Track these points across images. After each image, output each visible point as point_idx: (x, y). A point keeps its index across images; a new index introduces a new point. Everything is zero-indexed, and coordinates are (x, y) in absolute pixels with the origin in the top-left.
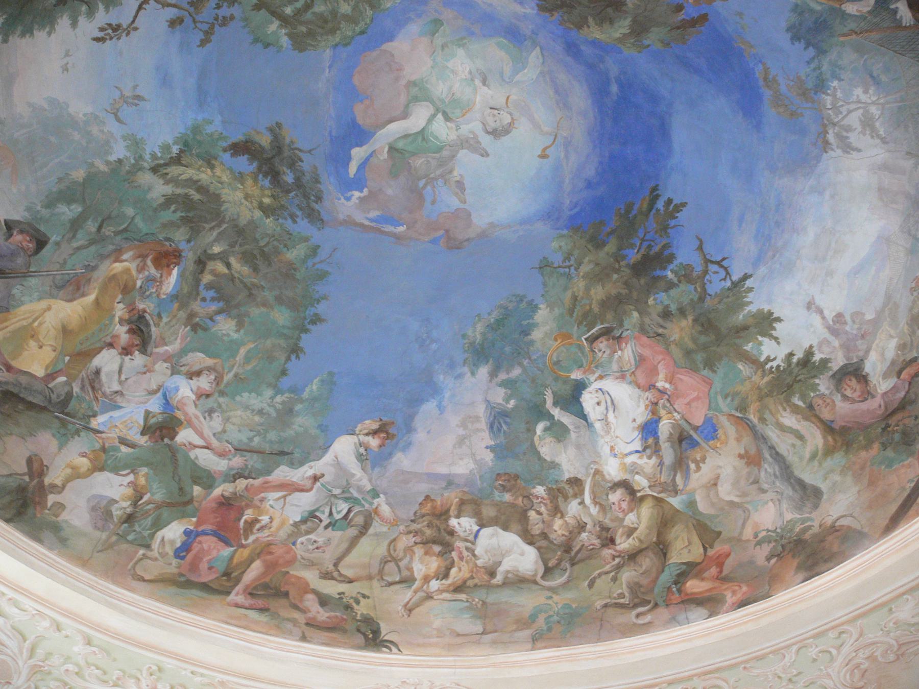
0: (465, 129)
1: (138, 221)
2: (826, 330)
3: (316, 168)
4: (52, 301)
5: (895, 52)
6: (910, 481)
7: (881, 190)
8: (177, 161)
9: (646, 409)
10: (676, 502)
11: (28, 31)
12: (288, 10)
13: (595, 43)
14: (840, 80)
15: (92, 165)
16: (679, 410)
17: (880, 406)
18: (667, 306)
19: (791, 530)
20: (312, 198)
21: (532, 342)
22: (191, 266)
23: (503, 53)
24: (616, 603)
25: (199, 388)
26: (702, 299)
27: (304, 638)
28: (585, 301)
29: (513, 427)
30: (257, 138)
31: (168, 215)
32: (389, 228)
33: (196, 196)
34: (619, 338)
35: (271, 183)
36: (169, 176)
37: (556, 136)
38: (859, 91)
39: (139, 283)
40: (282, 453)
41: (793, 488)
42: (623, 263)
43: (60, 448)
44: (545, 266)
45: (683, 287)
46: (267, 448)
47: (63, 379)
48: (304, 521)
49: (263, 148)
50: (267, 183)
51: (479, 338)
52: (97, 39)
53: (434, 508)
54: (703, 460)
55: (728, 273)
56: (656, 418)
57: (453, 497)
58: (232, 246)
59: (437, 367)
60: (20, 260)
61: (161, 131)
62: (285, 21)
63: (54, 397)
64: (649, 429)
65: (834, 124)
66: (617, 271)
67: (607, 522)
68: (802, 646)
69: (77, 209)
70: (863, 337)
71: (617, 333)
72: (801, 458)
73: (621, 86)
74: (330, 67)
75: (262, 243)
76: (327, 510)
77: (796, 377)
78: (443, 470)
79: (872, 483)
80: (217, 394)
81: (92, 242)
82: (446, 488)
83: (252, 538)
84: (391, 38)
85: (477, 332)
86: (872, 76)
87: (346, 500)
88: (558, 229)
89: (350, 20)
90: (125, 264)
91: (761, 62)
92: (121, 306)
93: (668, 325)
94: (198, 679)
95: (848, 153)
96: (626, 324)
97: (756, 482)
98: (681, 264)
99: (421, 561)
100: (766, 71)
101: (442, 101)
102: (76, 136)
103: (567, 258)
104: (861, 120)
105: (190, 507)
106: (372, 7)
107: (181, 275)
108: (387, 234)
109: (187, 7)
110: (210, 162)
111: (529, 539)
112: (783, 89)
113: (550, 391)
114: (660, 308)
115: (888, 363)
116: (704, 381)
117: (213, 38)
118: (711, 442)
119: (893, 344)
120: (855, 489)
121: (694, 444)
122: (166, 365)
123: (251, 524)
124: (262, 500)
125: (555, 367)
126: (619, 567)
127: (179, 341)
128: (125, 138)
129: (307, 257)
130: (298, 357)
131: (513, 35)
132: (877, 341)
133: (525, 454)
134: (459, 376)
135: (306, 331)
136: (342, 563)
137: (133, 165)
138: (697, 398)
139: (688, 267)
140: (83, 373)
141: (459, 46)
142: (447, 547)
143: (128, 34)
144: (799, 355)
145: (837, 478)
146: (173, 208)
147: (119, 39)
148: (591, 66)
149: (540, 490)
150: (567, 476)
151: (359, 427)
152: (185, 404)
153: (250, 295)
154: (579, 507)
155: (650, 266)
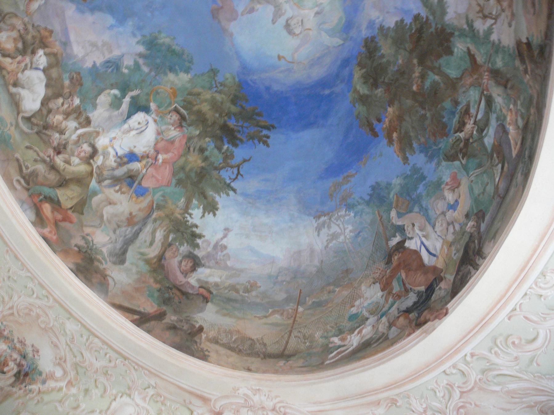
2: (215, 242)
5: (374, 241)
6: (145, 309)
7: (299, 252)
9: (144, 152)
10: (93, 184)
13: (351, 75)
14: (355, 217)
16: (148, 171)
17: (181, 282)
19: (96, 253)
21: (166, 74)
24: (21, 166)
26: (216, 168)
28: (198, 101)
29: (111, 74)
34: (181, 126)
38: (350, 227)
41: (120, 249)
42: (226, 118)
44: (214, 72)
51: (161, 41)
53: (46, 37)
54: (123, 193)
55: (234, 179)
56: (140, 159)
57: (57, 48)
59: (136, 19)
64: (132, 157)
65: (330, 219)
66: (221, 116)
67: (69, 147)
68: (32, 278)
70: (217, 263)
71: (184, 124)
72: (139, 248)
73: (329, 95)
78: (72, 37)
79: (137, 290)
85: (164, 39)
86: (359, 233)
88: (238, 75)
91: (357, 172)
93: (196, 153)
95: (316, 230)
96: (191, 129)
97: (119, 226)
98: (233, 152)
99: (8, 37)
100: (353, 176)
103: (222, 84)
104: (335, 232)
111: (45, 102)
112: (345, 187)
113: (139, 92)
114: (204, 146)
115: (205, 280)
116: (168, 182)
118: (134, 195)
119: (217, 279)
120: (130, 281)
121: (130, 185)
126: (44, 161)
131: (348, 26)
132: (216, 271)
133: (97, 86)
134: (134, 35)
138: (158, 180)
139: (232, 156)
142: (23, 52)
144: (198, 231)
145: (134, 270)
148: (337, 76)
150: (90, 115)
154: (74, 128)
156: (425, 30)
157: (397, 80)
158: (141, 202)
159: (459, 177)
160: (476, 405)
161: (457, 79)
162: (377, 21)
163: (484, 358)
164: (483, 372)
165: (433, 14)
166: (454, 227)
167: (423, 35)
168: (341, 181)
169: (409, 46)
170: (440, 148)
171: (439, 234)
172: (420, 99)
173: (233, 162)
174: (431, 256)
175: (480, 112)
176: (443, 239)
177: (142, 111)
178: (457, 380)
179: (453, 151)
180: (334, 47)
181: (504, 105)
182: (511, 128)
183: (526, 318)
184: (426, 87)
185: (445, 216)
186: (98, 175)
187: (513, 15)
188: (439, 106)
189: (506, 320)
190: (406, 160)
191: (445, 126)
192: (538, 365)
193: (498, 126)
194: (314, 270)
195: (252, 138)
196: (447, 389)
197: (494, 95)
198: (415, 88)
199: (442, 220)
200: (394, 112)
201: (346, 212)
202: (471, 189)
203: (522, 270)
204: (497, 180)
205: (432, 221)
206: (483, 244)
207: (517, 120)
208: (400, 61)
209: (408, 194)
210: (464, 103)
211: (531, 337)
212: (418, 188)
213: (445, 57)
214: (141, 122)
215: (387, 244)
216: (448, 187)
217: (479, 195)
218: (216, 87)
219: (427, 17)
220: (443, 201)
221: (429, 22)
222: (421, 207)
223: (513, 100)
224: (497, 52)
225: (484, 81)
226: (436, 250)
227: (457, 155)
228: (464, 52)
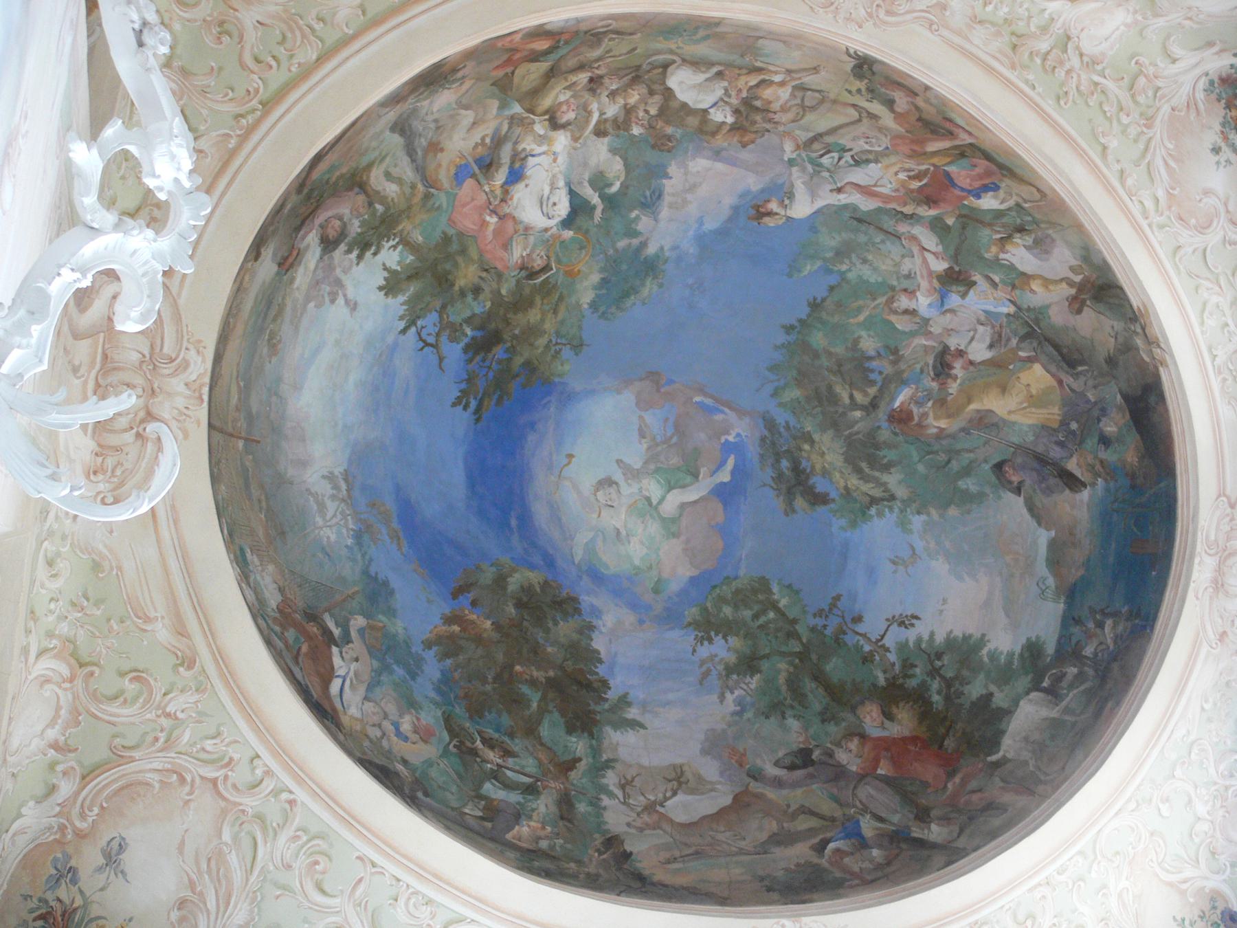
0: (635, 488)
1: (916, 459)
4: (1006, 417)
7: (303, 439)
8: (874, 501)
10: (517, 109)
11: (966, 638)
12: (771, 615)
13: (532, 567)
14: (347, 546)
15: (942, 516)
18: (475, 299)
21: (602, 270)
22: (883, 405)
23: (604, 558)
25: (911, 300)
26: (444, 307)
27: (927, 88)
28: (547, 308)
29: (642, 191)
32: (709, 401)
33: (864, 465)
35: (800, 463)
38: (333, 537)
39: (930, 404)
40: (860, 221)
42: (509, 344)
43: (1048, 306)
44: (578, 347)
45: (458, 319)
46: (872, 230)
47: (1021, 354)
48: (868, 161)
49: (802, 496)
50: (804, 464)
51: (648, 282)
52: (917, 618)
54: (477, 145)
55: (419, 334)
57: (720, 141)
58: (844, 414)
60: (1019, 460)
61: (881, 529)
62: (774, 606)
63: (1035, 344)
64: (516, 176)
66: (515, 337)
69: (962, 484)
71: (524, 273)
73: (509, 526)
74: (741, 559)
76: (842, 162)
78: (719, 166)
81: (958, 452)
82: (723, 149)
83: (923, 167)
84: (693, 581)
85: (649, 288)
87: (820, 165)
90: (936, 423)
92: (950, 391)
93: (476, 280)
94: (1031, 77)
96: (513, 282)
99: (778, 98)
100: (400, 549)
101: (653, 518)
102: (947, 544)
103: (558, 352)
105: (964, 212)
106: (706, 609)
107: (893, 399)
108: (712, 397)
110: (847, 493)
111: (669, 93)
112: (384, 531)
114: (481, 297)
121: (478, 161)
123: (918, 177)
124: (897, 190)
128: (910, 532)
129: (783, 388)
130: (815, 299)
131: (597, 577)
134: (675, 248)
135: (800, 321)
136: (853, 119)
138: (464, 206)
139: (453, 339)
140: (1003, 350)
141: (638, 568)
142: (747, 102)
144: (368, 254)
146: (885, 461)
149: (636, 131)
150: (606, 140)
151: (781, 222)
153: (840, 365)
155: (485, 341)
158: (449, 170)
160: (187, 802)
162: (600, 622)
163: (286, 819)
164: (260, 818)
165: (612, 710)
169: (569, 666)
172: (506, 676)
173: (444, 339)
177: (568, 216)
178: (241, 775)
183: (360, 880)
186: (522, 119)
189: (357, 854)
190: (428, 645)
192: (277, 897)
196: (220, 759)
198: (518, 668)
203: (436, 876)
211: (326, 887)
218: (557, 344)
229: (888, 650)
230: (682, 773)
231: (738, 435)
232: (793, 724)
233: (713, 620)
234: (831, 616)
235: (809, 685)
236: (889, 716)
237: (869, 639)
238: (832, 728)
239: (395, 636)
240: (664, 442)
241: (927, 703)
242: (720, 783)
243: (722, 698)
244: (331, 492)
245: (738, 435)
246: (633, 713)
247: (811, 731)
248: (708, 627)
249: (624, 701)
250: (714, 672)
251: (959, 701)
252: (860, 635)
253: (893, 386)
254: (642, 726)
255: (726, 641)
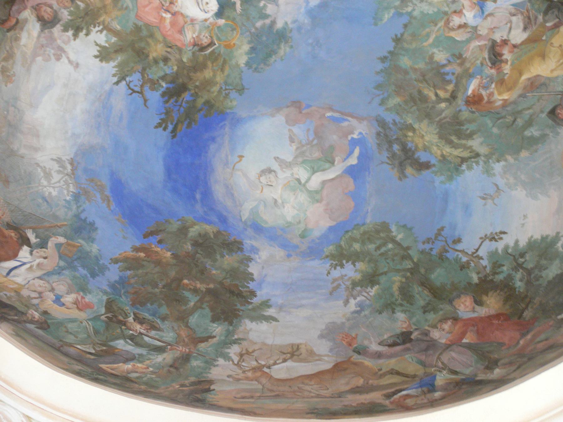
0: (288, 173)
1: (490, 125)
2: (66, 50)
3: (380, 153)
7: (38, 136)
8: (464, 160)
11: (544, 238)
12: (390, 246)
13: (210, 223)
14: (65, 200)
15: (515, 159)
18: (165, 65)
20: (382, 135)
21: (249, 42)
25: (460, 17)
26: (144, 69)
28: (216, 68)
30: (414, 172)
31: (471, 127)
32: (336, 115)
33: (454, 138)
34: (195, 45)
35: (407, 145)
36: (469, 150)
37: (233, 169)
38: (54, 193)
39: (493, 86)
42: (193, 92)
44: (241, 90)
47: (549, 24)
50: (409, 145)
51: (282, 46)
52: (504, 233)
55: (128, 86)
58: (433, 107)
59: (309, 28)
61: (472, 178)
62: (393, 240)
65: (67, 175)
66: (197, 87)
69: (527, 133)
70: (42, 46)
71: (196, 48)
73: (194, 198)
74: (368, 212)
75: (415, 108)
77: (83, 21)
80: (449, 13)
81: (520, 112)
84: (331, 229)
85: (284, 49)
88: (233, 113)
89: (354, 240)
90: (500, 97)
91: (112, 211)
92: (505, 72)
93: (164, 53)
95: (59, 158)
96: (190, 54)
98: (157, 91)
100: (108, 206)
101: (301, 191)
103: (227, 95)
104: (52, 177)
106: (340, 246)
107: (466, 89)
109: (450, 250)
110: (444, 159)
112: (98, 195)
113: (238, 11)
114: (170, 64)
115: (25, 28)
116: (141, 18)
117: (436, 232)
122: (481, 33)
125: (234, 27)
127: (471, 48)
128: (494, 175)
129: (387, 99)
130: (396, 36)
131: (258, 228)
134: (295, 22)
135: (390, 52)
137: (490, 158)
139: (153, 89)
140: (534, 28)
141: (290, 223)
143: (486, 236)
144: (82, 34)
146: (468, 131)
147: (492, 233)
148: (212, 209)
152: (471, 7)
155: (176, 90)
156: (240, 299)
157: (197, 266)
159: (89, 311)
161: (187, 322)
162: (257, 256)
165: (254, 309)
166: (35, 298)
167: (235, 297)
168: (106, 193)
169: (228, 282)
170: (121, 296)
171: (31, 282)
173: (146, 88)
174: (8, 270)
175: (150, 339)
176: (25, 285)
179: (116, 308)
180: (240, 211)
181: (153, 363)
182: (130, 366)
184: (184, 292)
185: (49, 291)
187: (238, 380)
188: (163, 302)
190: (115, 261)
191: (143, 304)
193: (134, 355)
194: (15, 147)
195: (167, 113)
197: (165, 355)
198: (186, 281)
199: (45, 287)
200: (165, 257)
201: (72, 192)
202: (73, 321)
204: (79, 347)
205: (46, 277)
206: (11, 323)
207: (137, 372)
208: (214, 272)
209: (79, 258)
210: (162, 326)
212: (84, 269)
213: (210, 314)
214: (208, 6)
215: (30, 228)
216: (79, 298)
217: (65, 327)
219: (252, 303)
220: (66, 292)
221: (247, 305)
222: (63, 269)
223: (157, 371)
224: (206, 362)
225: (181, 347)
226: (14, 276)
227: (111, 312)
228: (212, 333)
229: (482, 258)
230: (298, 349)
231: (360, 133)
232: (401, 316)
233: (345, 253)
234: (436, 242)
235: (416, 289)
236: (478, 302)
237: (467, 253)
238: (431, 317)
239: (87, 253)
240: (307, 144)
241: (513, 289)
242: (328, 356)
243: (346, 302)
244: (58, 169)
245: (360, 133)
246: (271, 312)
247: (414, 320)
248: (340, 257)
249: (266, 304)
250: (343, 286)
251: (537, 283)
252: (460, 251)
253: (464, 81)
254: (275, 320)
255: (354, 265)
